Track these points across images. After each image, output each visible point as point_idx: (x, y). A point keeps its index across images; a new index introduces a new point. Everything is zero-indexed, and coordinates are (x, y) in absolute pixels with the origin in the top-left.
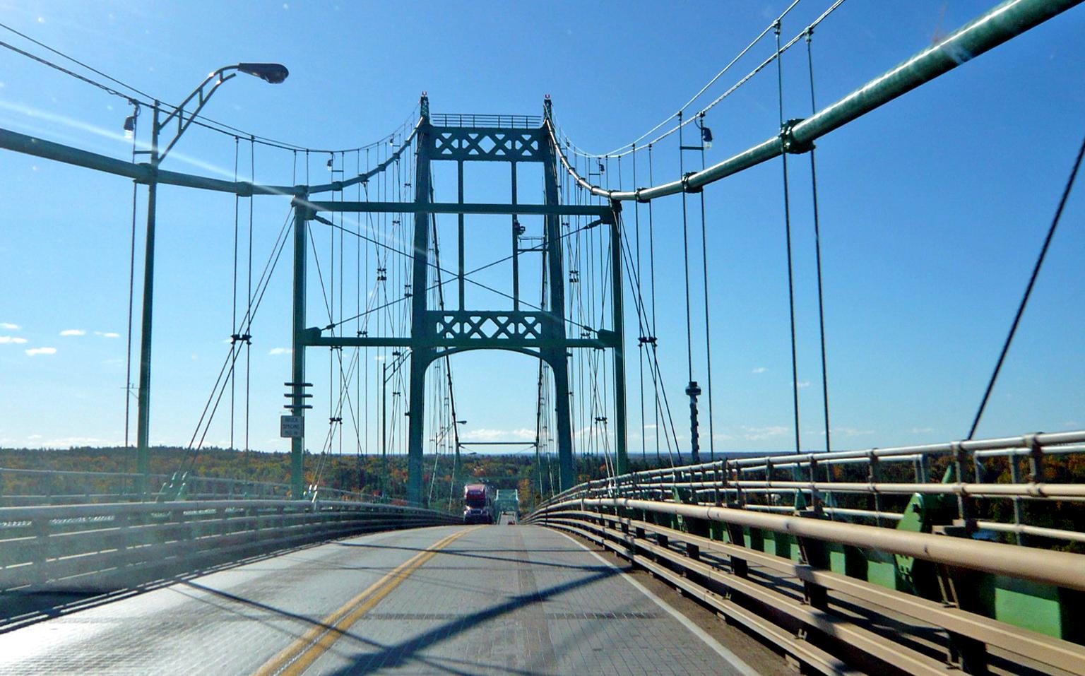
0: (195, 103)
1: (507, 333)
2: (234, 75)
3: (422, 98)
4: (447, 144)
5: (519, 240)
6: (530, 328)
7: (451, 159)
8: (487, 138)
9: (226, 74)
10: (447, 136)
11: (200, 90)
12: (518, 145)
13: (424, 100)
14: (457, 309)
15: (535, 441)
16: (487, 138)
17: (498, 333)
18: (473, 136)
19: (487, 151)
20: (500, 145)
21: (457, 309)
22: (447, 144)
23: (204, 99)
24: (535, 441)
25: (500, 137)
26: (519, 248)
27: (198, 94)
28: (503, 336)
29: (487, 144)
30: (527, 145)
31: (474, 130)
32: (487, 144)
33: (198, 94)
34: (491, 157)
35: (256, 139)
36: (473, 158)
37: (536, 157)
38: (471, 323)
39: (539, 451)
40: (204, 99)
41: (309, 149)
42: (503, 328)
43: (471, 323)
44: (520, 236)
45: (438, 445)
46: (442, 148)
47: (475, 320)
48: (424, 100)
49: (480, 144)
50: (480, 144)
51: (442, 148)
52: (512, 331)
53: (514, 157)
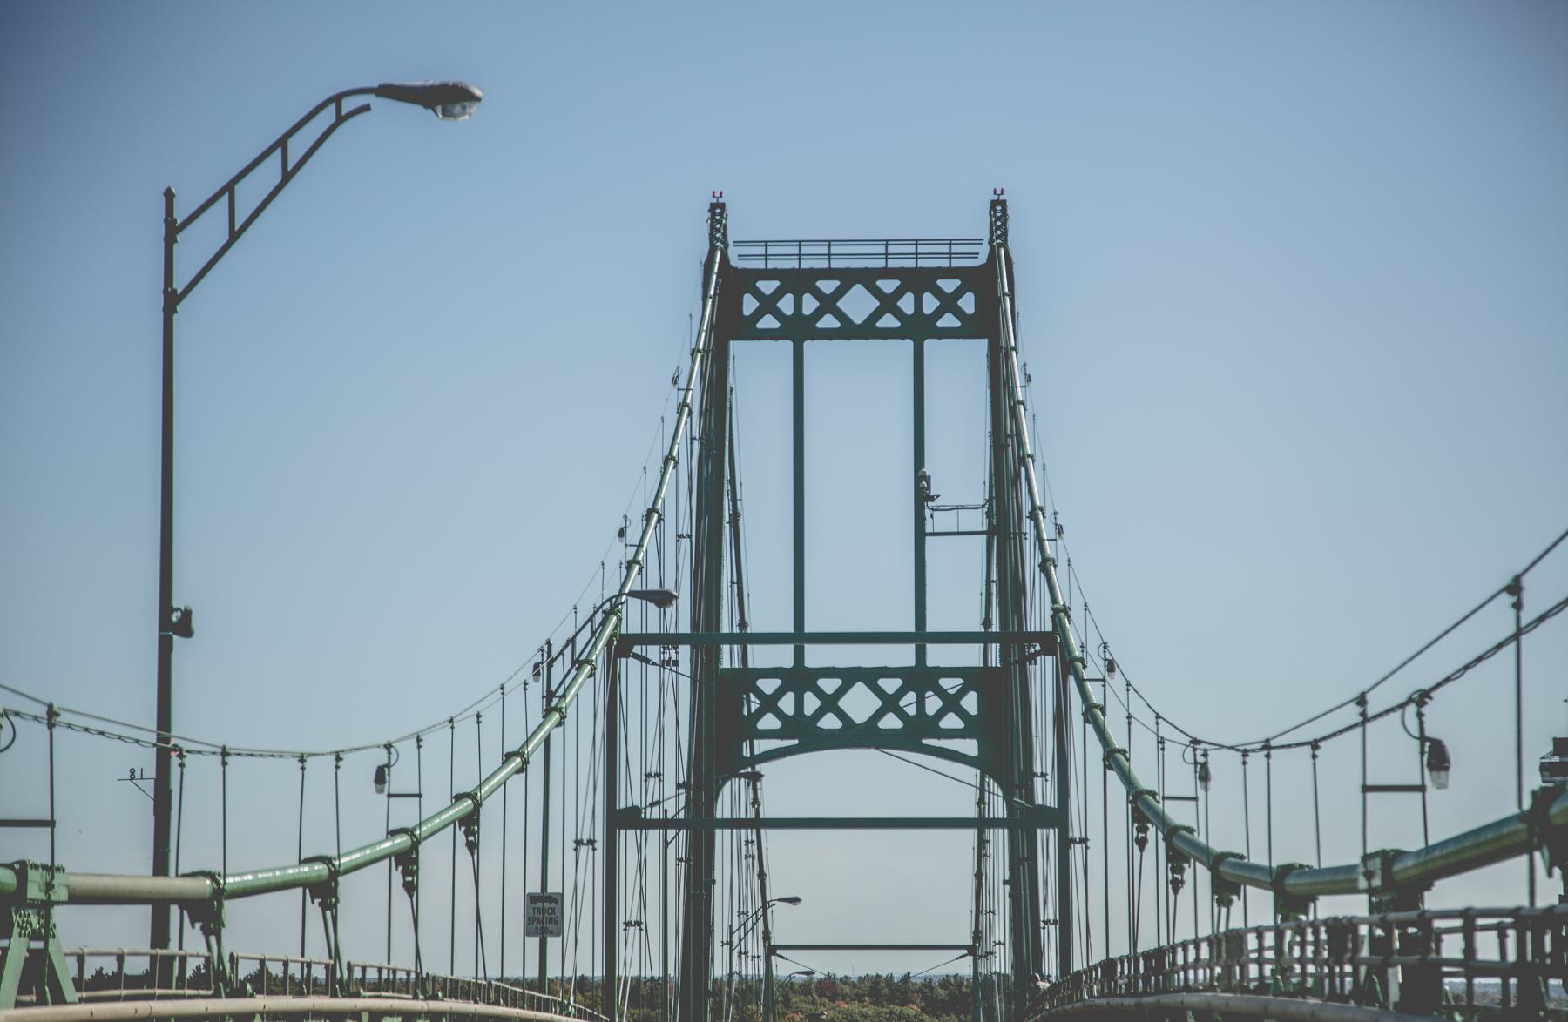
0: (271, 171)
1: (900, 713)
2: (366, 108)
3: (712, 205)
4: (768, 305)
5: (928, 513)
6: (952, 703)
7: (776, 338)
8: (860, 689)
9: (349, 104)
10: (768, 287)
11: (282, 143)
12: (930, 303)
13: (717, 211)
14: (808, 344)
15: (969, 942)
16: (860, 689)
17: (879, 715)
18: (827, 287)
19: (858, 319)
20: (888, 304)
21: (808, 344)
22: (768, 305)
23: (237, 228)
24: (969, 942)
25: (888, 286)
26: (928, 529)
27: (224, 200)
28: (891, 722)
29: (858, 304)
30: (949, 303)
31: (829, 274)
32: (858, 304)
33: (223, 202)
34: (868, 330)
35: (64, 717)
36: (829, 334)
37: (969, 329)
38: (819, 693)
39: (982, 970)
40: (237, 228)
41: (231, 745)
42: (890, 703)
43: (819, 693)
44: (930, 504)
45: (735, 954)
46: (758, 315)
47: (888, 321)
48: (717, 211)
49: (841, 304)
50: (841, 304)
51: (758, 315)
52: (912, 711)
53: (918, 329)
